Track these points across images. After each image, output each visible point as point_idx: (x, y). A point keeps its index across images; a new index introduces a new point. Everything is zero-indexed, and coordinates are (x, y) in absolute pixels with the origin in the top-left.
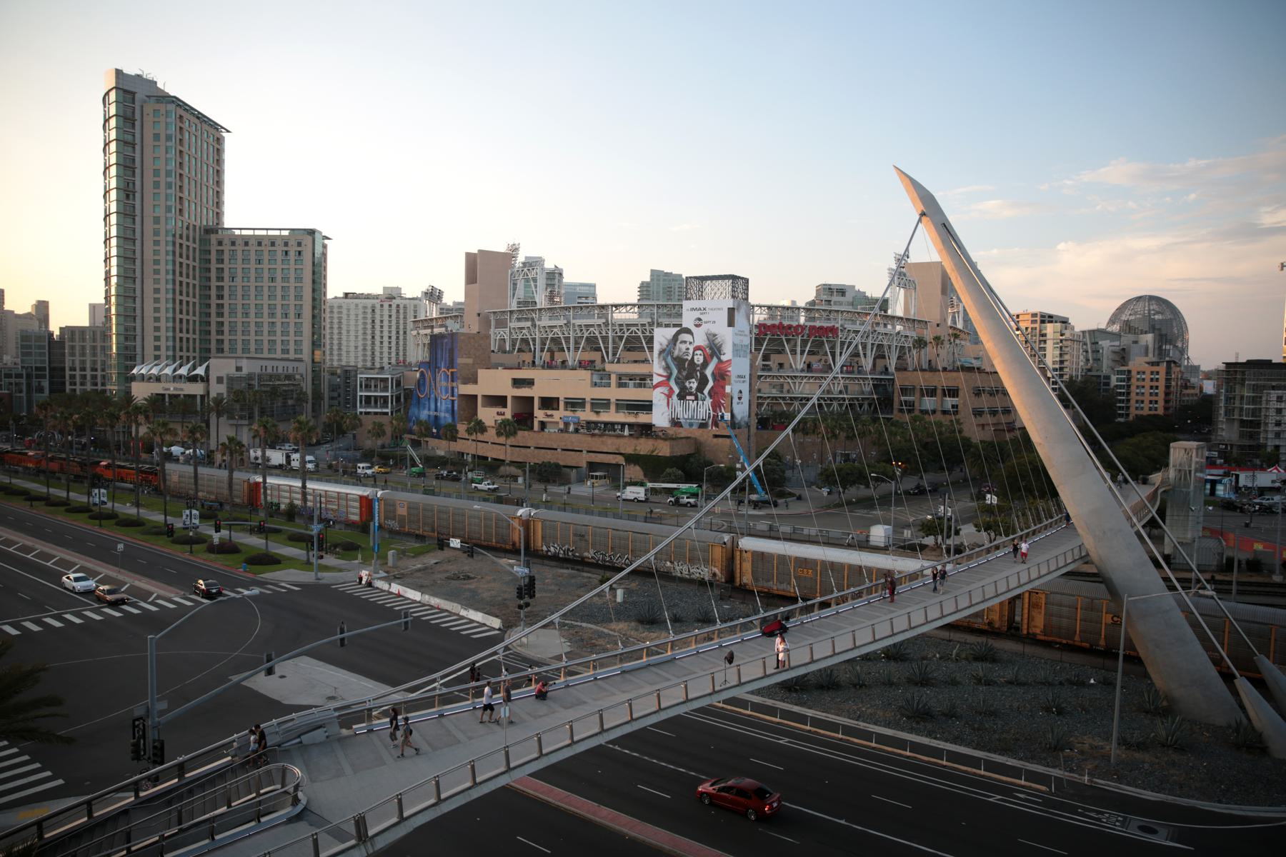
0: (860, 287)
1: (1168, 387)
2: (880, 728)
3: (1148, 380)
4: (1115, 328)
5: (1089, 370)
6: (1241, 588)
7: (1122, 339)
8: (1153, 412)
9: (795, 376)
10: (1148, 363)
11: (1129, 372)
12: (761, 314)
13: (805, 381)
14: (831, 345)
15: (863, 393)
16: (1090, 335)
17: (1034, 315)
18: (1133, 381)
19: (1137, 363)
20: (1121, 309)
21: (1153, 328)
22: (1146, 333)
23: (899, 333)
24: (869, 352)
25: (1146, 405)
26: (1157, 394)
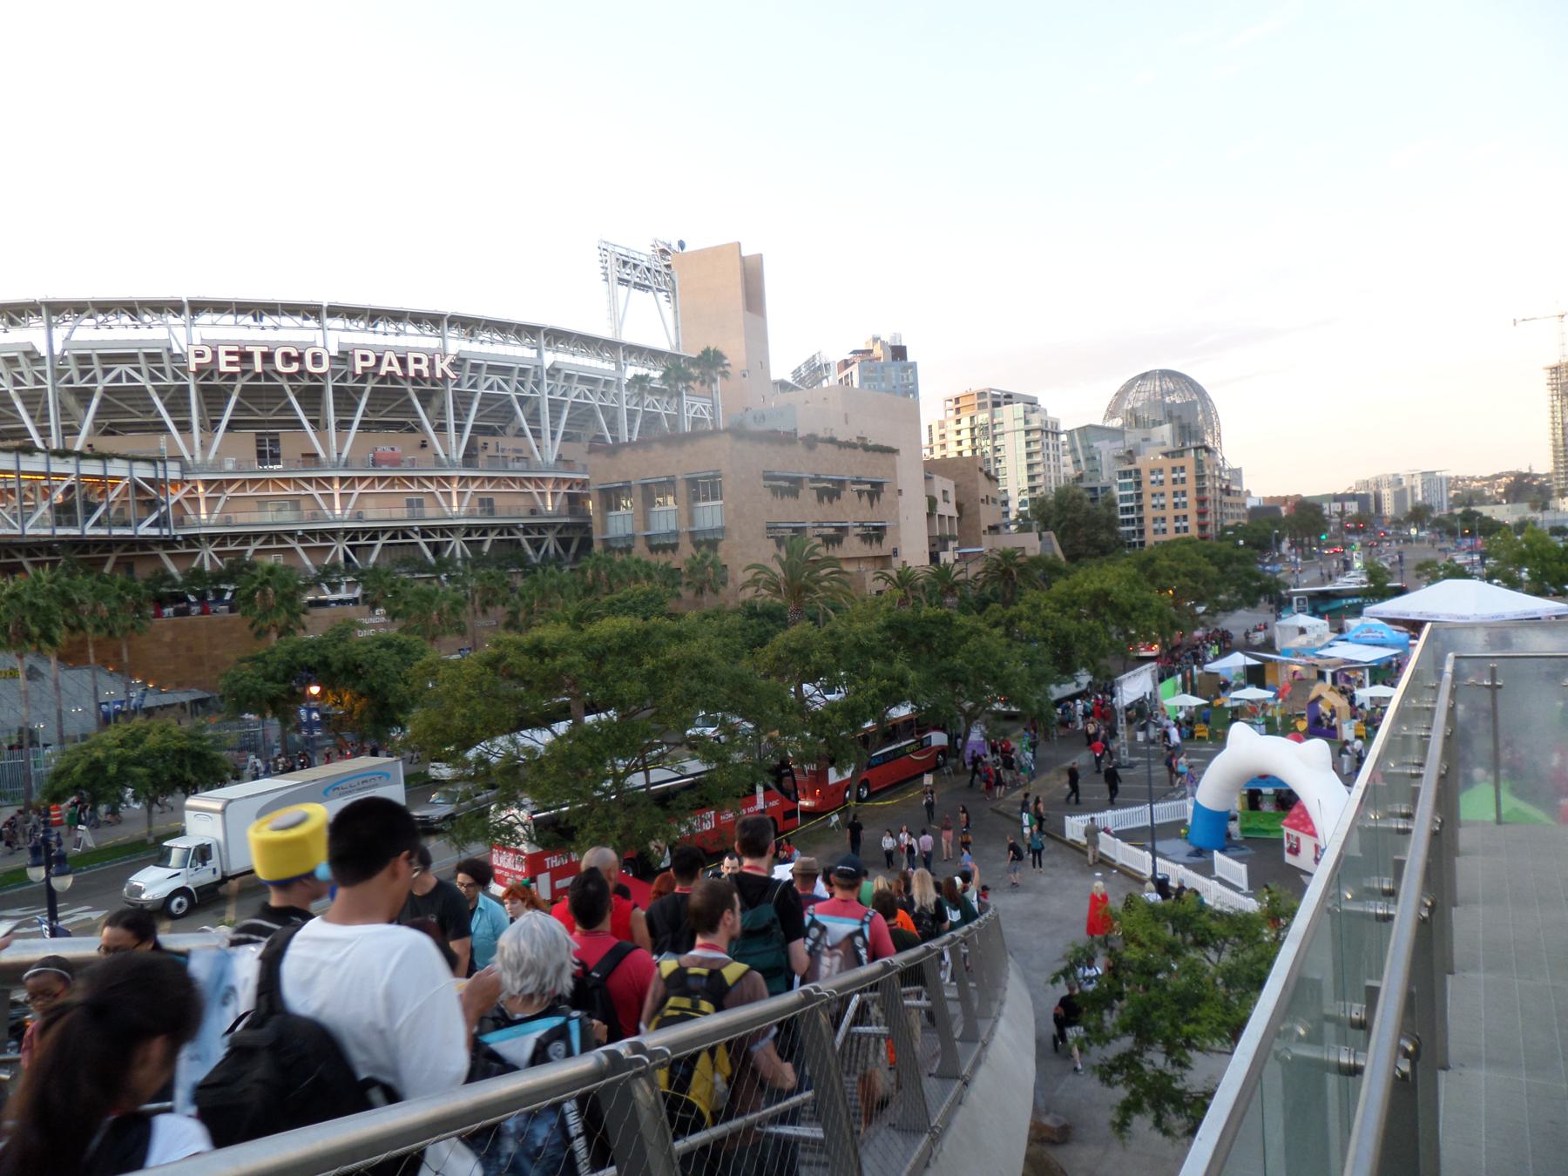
1: (1202, 501)
3: (1168, 483)
4: (1117, 423)
5: (1080, 478)
8: (1182, 535)
9: (325, 479)
10: (1166, 454)
11: (1138, 471)
13: (359, 489)
14: (528, 409)
16: (1079, 435)
17: (982, 394)
18: (1146, 486)
19: (1150, 458)
20: (1121, 395)
21: (1170, 417)
22: (1160, 424)
25: (1170, 525)
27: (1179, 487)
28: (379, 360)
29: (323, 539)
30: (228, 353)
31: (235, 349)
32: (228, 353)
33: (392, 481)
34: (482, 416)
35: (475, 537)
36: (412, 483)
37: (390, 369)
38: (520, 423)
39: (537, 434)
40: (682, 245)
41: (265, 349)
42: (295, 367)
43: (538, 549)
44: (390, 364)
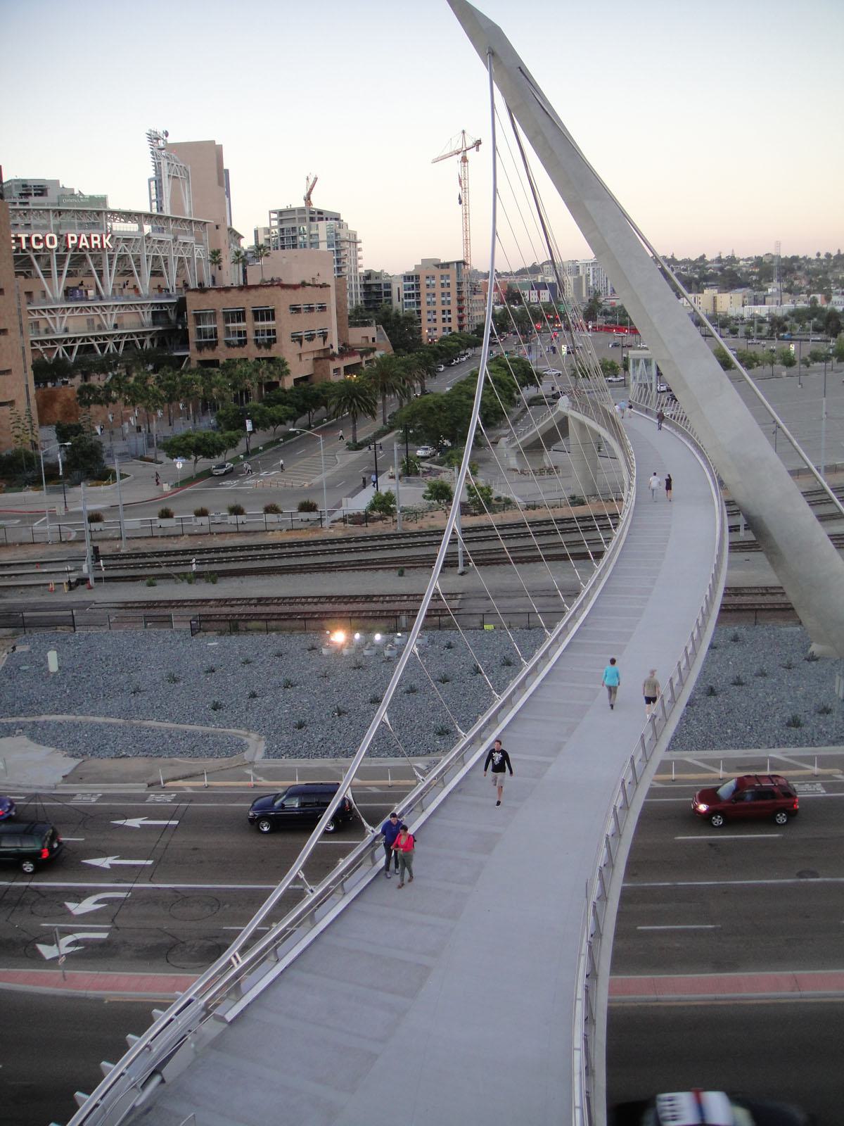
0: (66, 183)
2: (823, 748)
6: (468, 535)
9: (53, 309)
13: (67, 314)
15: (143, 325)
23: (148, 237)
24: (106, 269)
26: (449, 302)
27: (446, 290)
29: (52, 344)
33: (82, 309)
35: (69, 344)
37: (84, 244)
39: (100, 274)
40: (167, 134)
42: (41, 246)
43: (102, 351)
44: (84, 241)
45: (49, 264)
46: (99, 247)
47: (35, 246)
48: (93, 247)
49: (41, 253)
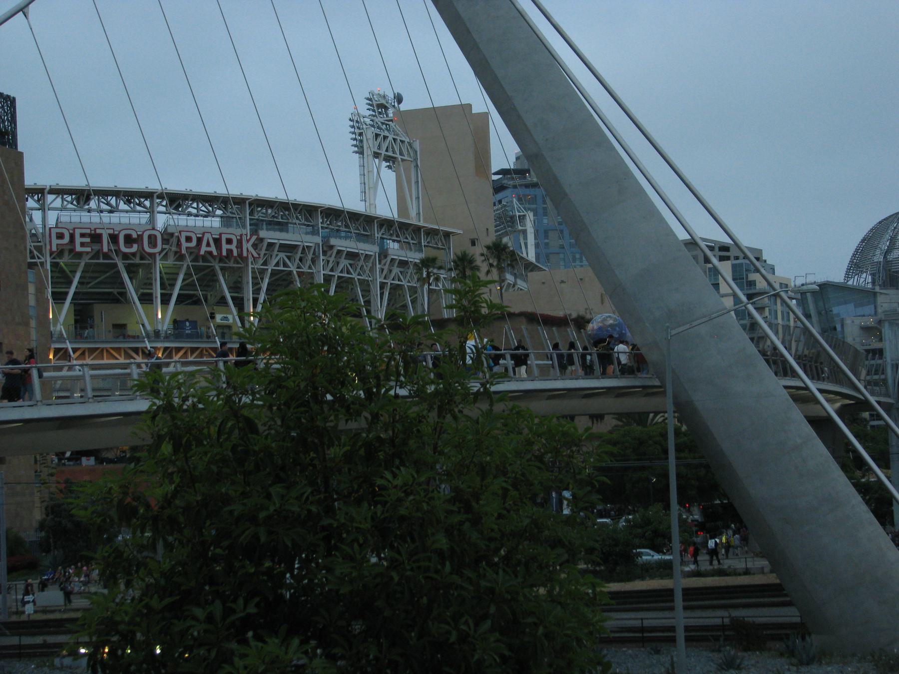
4: (864, 280)
7: (880, 299)
12: (63, 209)
24: (249, 294)
28: (200, 240)
30: (82, 235)
31: (88, 231)
32: (82, 235)
34: (185, 285)
36: (137, 354)
37: (208, 249)
38: (222, 291)
40: (399, 99)
41: (111, 232)
42: (135, 248)
44: (208, 245)
45: (149, 284)
46: (235, 254)
47: (123, 249)
48: (224, 253)
49: (137, 261)
